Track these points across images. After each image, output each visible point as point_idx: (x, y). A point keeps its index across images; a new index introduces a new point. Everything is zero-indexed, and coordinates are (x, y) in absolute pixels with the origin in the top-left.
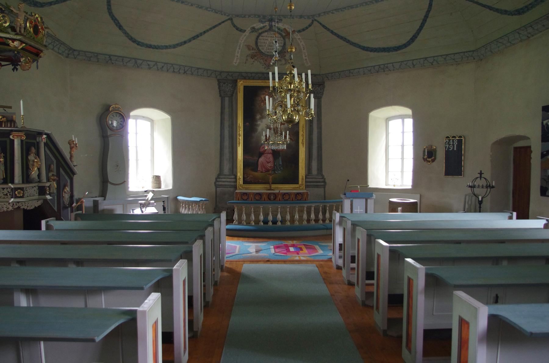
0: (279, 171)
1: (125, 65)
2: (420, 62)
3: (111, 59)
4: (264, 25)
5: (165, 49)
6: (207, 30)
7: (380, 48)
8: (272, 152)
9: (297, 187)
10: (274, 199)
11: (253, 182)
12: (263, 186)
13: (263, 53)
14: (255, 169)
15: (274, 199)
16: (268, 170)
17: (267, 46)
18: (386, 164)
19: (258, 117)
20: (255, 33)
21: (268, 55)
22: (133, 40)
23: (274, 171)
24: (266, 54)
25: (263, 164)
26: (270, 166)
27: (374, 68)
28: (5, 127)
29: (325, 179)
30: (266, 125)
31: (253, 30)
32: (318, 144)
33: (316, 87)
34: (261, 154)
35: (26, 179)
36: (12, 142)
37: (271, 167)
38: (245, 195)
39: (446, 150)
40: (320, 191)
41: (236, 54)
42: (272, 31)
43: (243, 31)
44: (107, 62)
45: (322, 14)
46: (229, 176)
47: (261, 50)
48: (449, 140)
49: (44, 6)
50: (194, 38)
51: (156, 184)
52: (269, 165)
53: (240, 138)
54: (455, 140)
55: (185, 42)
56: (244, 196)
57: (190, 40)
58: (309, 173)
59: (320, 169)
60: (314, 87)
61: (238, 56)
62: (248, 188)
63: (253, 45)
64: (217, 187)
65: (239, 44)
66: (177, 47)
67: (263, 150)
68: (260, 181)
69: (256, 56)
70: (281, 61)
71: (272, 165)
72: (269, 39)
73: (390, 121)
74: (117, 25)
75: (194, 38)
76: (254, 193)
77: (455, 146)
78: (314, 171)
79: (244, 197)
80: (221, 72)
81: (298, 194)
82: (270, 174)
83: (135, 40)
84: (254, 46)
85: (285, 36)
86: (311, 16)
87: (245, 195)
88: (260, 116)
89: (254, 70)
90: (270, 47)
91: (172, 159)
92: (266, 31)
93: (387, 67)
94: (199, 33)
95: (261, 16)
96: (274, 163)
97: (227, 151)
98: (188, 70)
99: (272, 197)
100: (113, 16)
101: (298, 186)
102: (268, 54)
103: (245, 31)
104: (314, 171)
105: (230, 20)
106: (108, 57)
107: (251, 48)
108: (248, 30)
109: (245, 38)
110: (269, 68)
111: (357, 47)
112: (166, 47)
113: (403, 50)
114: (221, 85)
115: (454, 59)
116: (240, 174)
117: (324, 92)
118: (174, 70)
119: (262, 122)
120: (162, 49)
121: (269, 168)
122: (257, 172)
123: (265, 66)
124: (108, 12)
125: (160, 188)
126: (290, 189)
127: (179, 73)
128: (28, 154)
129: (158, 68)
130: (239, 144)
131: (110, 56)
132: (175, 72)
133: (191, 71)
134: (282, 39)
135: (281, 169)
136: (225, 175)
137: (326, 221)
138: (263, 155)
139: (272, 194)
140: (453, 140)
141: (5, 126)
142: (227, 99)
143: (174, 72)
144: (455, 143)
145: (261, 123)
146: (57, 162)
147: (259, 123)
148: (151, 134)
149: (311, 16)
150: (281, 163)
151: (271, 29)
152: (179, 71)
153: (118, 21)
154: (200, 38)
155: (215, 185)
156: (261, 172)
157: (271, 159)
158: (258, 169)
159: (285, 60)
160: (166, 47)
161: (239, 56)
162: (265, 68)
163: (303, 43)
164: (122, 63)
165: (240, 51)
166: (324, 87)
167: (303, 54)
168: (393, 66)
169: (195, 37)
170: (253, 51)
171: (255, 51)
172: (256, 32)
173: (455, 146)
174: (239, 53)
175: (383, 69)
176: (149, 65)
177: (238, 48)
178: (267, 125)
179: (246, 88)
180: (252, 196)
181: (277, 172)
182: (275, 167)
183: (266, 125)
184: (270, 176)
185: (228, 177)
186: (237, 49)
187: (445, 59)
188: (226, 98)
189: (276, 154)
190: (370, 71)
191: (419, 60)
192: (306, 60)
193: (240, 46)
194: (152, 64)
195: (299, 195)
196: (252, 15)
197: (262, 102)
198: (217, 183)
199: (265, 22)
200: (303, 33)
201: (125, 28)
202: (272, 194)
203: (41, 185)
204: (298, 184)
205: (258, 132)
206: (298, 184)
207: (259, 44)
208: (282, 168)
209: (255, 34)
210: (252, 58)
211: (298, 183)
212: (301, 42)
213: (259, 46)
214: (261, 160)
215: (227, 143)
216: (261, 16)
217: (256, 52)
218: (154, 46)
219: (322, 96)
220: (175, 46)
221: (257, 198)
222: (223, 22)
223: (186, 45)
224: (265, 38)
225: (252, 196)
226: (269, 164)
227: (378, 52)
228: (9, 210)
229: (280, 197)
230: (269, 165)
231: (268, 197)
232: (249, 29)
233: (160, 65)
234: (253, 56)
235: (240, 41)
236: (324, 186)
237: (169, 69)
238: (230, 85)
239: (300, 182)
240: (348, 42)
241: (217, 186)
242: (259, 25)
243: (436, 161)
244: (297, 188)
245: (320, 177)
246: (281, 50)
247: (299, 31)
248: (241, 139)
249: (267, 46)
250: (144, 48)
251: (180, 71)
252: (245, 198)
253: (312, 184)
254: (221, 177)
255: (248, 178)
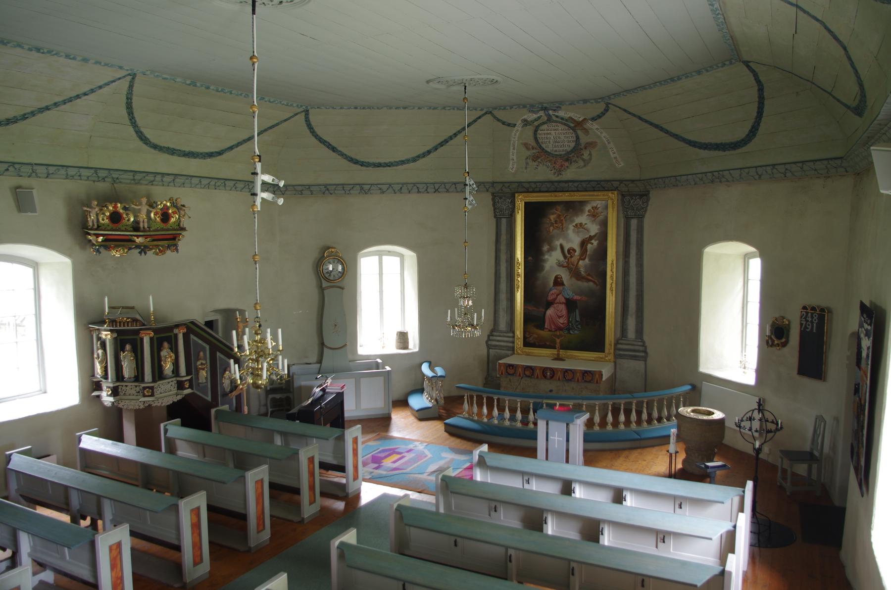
0: (576, 330)
1: (348, 194)
2: (766, 172)
3: (328, 190)
4: (539, 115)
5: (402, 164)
6: (459, 131)
7: (711, 144)
8: (564, 302)
9: (601, 356)
10: (552, 377)
11: (537, 344)
12: (550, 352)
13: (548, 152)
14: (541, 326)
15: (552, 377)
16: (560, 329)
17: (552, 142)
18: (742, 332)
19: (545, 248)
20: (530, 126)
21: (556, 155)
22: (355, 161)
23: (569, 330)
24: (553, 154)
25: (552, 319)
26: (562, 322)
27: (706, 175)
28: (131, 327)
29: (646, 347)
30: (557, 260)
31: (526, 123)
32: (637, 290)
33: (636, 200)
34: (549, 304)
35: (158, 374)
36: (142, 340)
37: (564, 323)
38: (511, 367)
39: (802, 329)
40: (639, 365)
41: (511, 157)
42: (552, 122)
43: (513, 125)
44: (324, 193)
45: (612, 97)
46: (506, 333)
47: (545, 148)
48: (807, 313)
49: (223, 153)
50: (441, 144)
51: (400, 343)
52: (561, 321)
53: (519, 279)
54: (815, 314)
55: (429, 152)
56: (510, 368)
57: (436, 148)
58: (622, 337)
59: (639, 331)
60: (632, 199)
61: (513, 160)
62: (530, 353)
63: (532, 143)
64: (490, 348)
65: (512, 142)
66: (418, 160)
67: (552, 298)
68: (548, 344)
69: (539, 158)
70: (577, 162)
71: (565, 322)
72: (553, 132)
73: (751, 259)
74: (329, 148)
75: (441, 144)
76: (524, 365)
77: (815, 324)
78: (631, 334)
79: (509, 371)
80: (493, 183)
81: (586, 372)
82: (558, 337)
83: (357, 160)
84: (533, 143)
85: (575, 126)
86: (600, 99)
87: (511, 367)
88: (548, 247)
89: (540, 178)
90: (556, 144)
91: (419, 312)
92: (544, 123)
93: (723, 176)
94: (447, 137)
95: (528, 106)
96: (569, 318)
97: (503, 296)
98: (439, 187)
99: (548, 374)
100: (321, 138)
101: (604, 356)
102: (556, 153)
103: (516, 125)
104: (631, 334)
105: (488, 114)
106: (324, 187)
107: (531, 147)
108: (519, 123)
109: (518, 134)
110: (561, 174)
111: (680, 141)
112: (403, 162)
113: (743, 148)
114: (497, 200)
115: (815, 170)
116: (519, 332)
117: (649, 208)
118: (418, 190)
119: (550, 256)
120: (397, 166)
121: (561, 325)
122: (543, 330)
123: (555, 171)
124: (313, 135)
125: (406, 348)
126: (591, 358)
127: (428, 193)
128: (160, 349)
129: (394, 191)
130: (518, 288)
131: (326, 186)
132: (420, 192)
133: (445, 187)
134: (571, 131)
135: (578, 328)
136: (501, 332)
137: (607, 427)
138: (553, 306)
139: (548, 369)
140: (812, 314)
141: (131, 325)
142: (504, 221)
143: (419, 192)
144: (815, 320)
145: (549, 258)
146: (210, 349)
147: (546, 257)
148: (401, 274)
149: (600, 99)
150: (578, 319)
151: (549, 119)
152: (427, 190)
153: (328, 143)
154: (451, 142)
155: (487, 345)
156: (550, 331)
157: (564, 312)
158: (544, 326)
159: (584, 160)
160: (403, 162)
161: (515, 159)
162: (555, 173)
163: (604, 134)
164: (344, 192)
165: (515, 151)
166: (648, 200)
167: (610, 150)
168: (730, 173)
169: (442, 142)
170: (534, 151)
171: (537, 151)
172: (530, 125)
173: (815, 324)
174: (515, 155)
175: (717, 178)
176: (380, 189)
177: (512, 148)
178: (559, 261)
179: (527, 205)
180: (520, 369)
181: (573, 331)
182: (570, 324)
183: (557, 260)
184: (557, 339)
185: (505, 334)
186: (511, 150)
187: (802, 168)
188: (502, 219)
189: (570, 304)
190: (701, 179)
191: (764, 168)
192: (616, 158)
193: (514, 145)
194: (384, 187)
195: (587, 374)
196: (514, 105)
197: (551, 226)
198: (490, 343)
199: (538, 111)
200: (599, 120)
201: (339, 149)
202: (548, 369)
203: (179, 379)
204: (604, 352)
205: (545, 272)
206: (604, 352)
207: (540, 141)
208: (579, 327)
209: (530, 130)
210: (535, 161)
211: (604, 351)
212: (601, 133)
213: (540, 142)
214: (550, 312)
215: (503, 286)
216: (528, 106)
217: (538, 152)
218: (385, 163)
219: (645, 214)
220: (414, 160)
221: (527, 373)
222: (479, 118)
223: (432, 155)
224: (546, 132)
225: (520, 369)
226: (561, 319)
227: (710, 149)
228: (141, 408)
229: (560, 375)
230: (561, 321)
231: (543, 372)
232: (520, 122)
233: (397, 187)
234: (535, 158)
235: (513, 139)
236: (645, 359)
237: (412, 189)
238: (508, 200)
239: (607, 351)
240: (667, 132)
241: (489, 347)
242: (531, 117)
243: (789, 345)
244: (602, 358)
245: (640, 343)
246: (575, 147)
247: (593, 119)
248: (520, 281)
249: (552, 142)
250: (371, 168)
251: (428, 190)
252: (511, 371)
253: (627, 353)
254: (495, 334)
255: (531, 339)
